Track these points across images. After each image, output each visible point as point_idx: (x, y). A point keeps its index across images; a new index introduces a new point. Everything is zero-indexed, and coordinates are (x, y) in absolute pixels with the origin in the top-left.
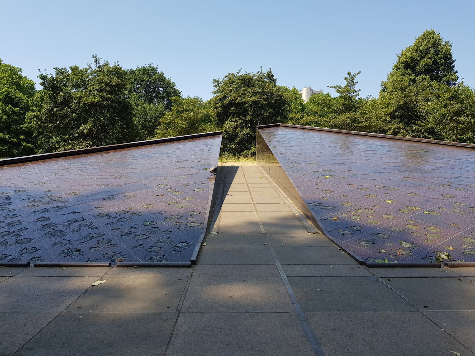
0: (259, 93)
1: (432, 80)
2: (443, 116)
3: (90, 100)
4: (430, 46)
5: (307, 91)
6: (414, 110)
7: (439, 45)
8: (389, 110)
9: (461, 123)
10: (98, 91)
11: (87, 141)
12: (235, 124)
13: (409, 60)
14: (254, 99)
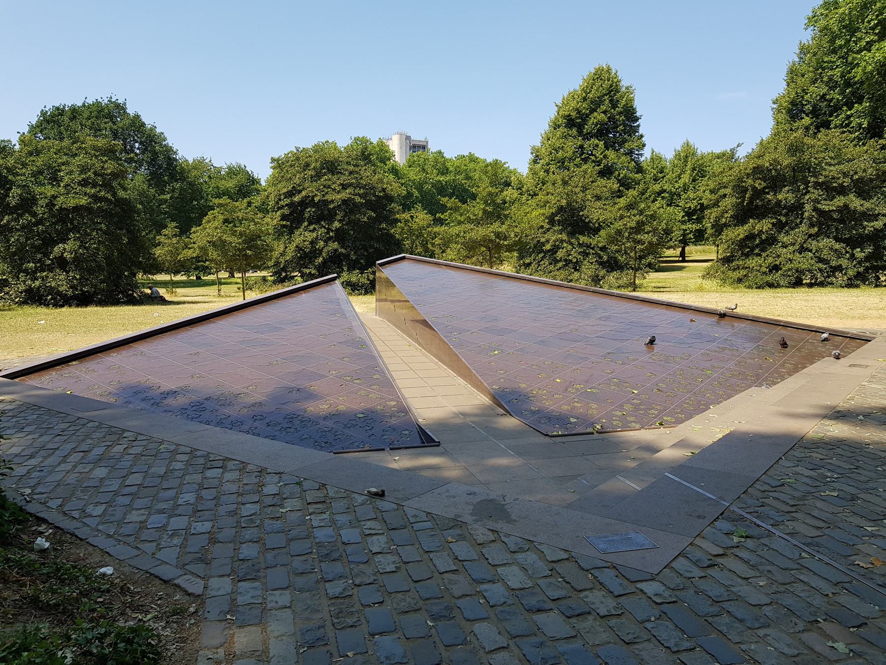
0: (351, 185)
1: (607, 148)
2: (619, 232)
3: (72, 202)
4: (604, 92)
5: (401, 139)
6: (581, 213)
7: (617, 91)
8: (548, 211)
9: (640, 242)
10: (82, 186)
11: (67, 272)
12: (315, 235)
13: (574, 114)
14: (344, 195)
